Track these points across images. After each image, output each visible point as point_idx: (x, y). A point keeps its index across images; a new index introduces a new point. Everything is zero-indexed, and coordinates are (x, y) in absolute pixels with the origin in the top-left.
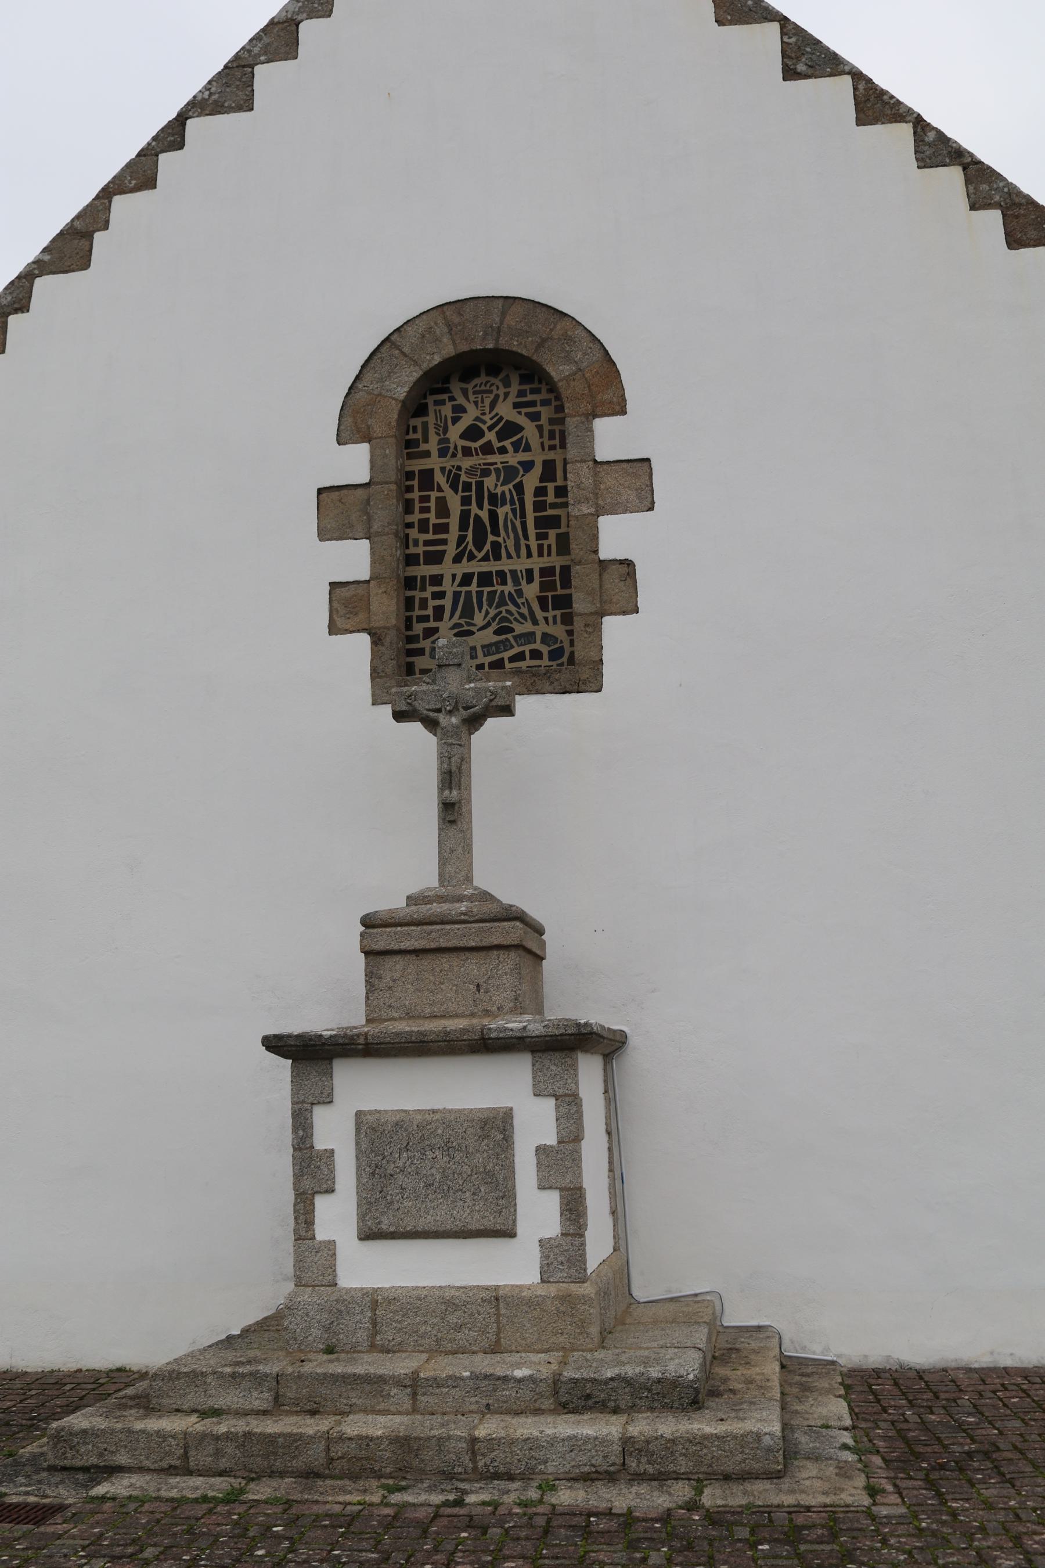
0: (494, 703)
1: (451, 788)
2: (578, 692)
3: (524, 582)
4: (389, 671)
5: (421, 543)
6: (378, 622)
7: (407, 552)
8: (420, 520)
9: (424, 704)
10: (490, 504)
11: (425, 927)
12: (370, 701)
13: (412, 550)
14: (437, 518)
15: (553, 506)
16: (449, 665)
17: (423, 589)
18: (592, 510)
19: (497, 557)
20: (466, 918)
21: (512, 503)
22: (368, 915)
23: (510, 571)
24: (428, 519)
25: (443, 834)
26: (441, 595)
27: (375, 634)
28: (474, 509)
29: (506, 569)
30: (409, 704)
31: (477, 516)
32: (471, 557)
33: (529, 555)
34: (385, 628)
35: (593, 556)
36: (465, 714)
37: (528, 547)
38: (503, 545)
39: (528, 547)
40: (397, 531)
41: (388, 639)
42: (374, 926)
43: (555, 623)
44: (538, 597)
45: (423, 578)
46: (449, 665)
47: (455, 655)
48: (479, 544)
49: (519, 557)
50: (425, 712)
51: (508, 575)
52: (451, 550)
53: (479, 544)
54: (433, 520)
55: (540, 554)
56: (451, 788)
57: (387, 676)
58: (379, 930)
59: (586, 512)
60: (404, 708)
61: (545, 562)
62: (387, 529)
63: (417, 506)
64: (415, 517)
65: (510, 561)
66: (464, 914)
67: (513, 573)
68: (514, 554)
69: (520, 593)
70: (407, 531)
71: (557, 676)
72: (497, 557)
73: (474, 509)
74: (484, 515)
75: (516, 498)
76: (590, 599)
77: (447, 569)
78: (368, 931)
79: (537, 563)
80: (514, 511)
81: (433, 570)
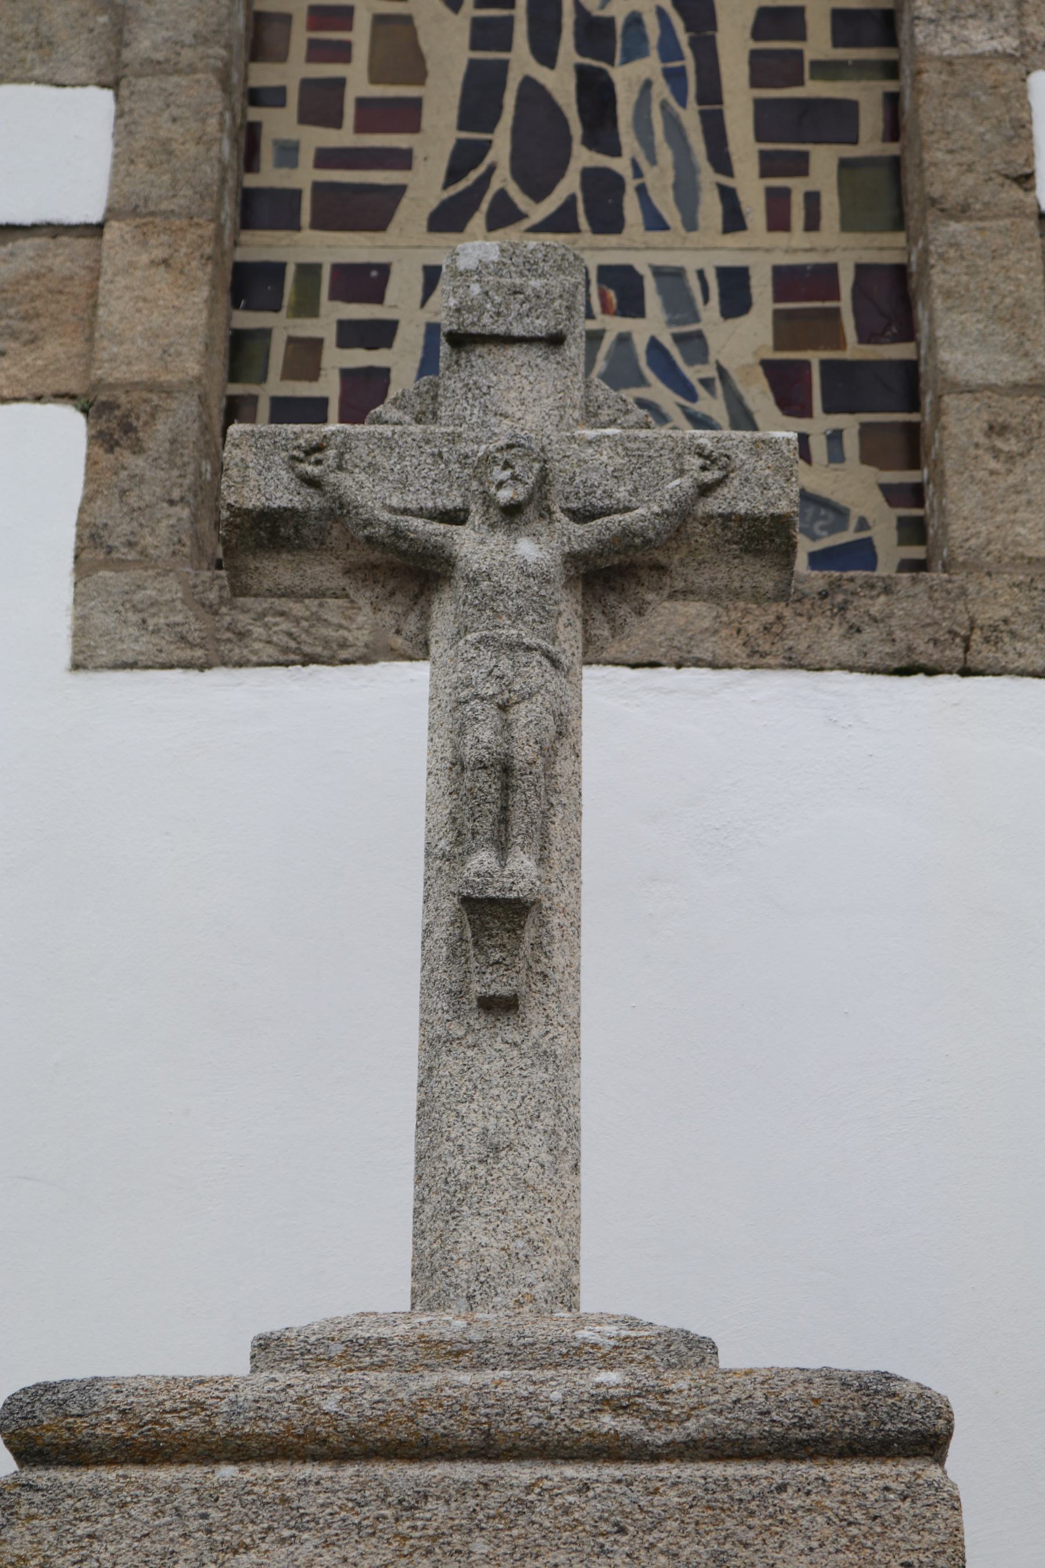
0: (714, 505)
1: (502, 848)
2: (966, 672)
3: (710, 312)
4: (156, 539)
5: (307, 157)
6: (123, 361)
7: (251, 181)
8: (307, 84)
9: (382, 489)
10: (581, 48)
11: (381, 1470)
12: (65, 653)
13: (269, 176)
14: (375, 79)
15: (825, 69)
16: (508, 340)
17: (307, 307)
18: (1010, 43)
19: (608, 221)
20: (629, 1425)
21: (669, 49)
22: (48, 1387)
23: (658, 272)
24: (339, 84)
25: (450, 1064)
26: (381, 334)
27: (109, 406)
28: (521, 61)
29: (642, 263)
30: (312, 483)
31: (530, 88)
32: (503, 215)
33: (734, 219)
34: (153, 387)
35: (1016, 193)
36: (582, 536)
37: (729, 197)
38: (631, 184)
39: (729, 197)
40: (227, 64)
41: (163, 428)
42: (76, 1454)
43: (836, 455)
44: (768, 366)
45: (309, 272)
46: (508, 340)
47: (538, 301)
48: (537, 171)
49: (691, 224)
50: (386, 516)
51: (650, 285)
52: (426, 186)
53: (537, 171)
54: (358, 81)
55: (778, 221)
56: (502, 848)
57: (145, 559)
58: (110, 1475)
59: (987, 46)
60: (282, 499)
61: (797, 247)
62: (187, 55)
63: (300, 37)
64: (292, 71)
65: (657, 237)
66: (617, 1406)
67: (670, 278)
68: (671, 213)
69: (695, 345)
70: (255, 114)
71: (878, 605)
72: (608, 221)
73: (521, 61)
74: (561, 84)
75: (683, 37)
76: (1012, 336)
77: (402, 247)
78: (41, 1476)
79: (761, 252)
80: (675, 78)
81: (355, 247)
